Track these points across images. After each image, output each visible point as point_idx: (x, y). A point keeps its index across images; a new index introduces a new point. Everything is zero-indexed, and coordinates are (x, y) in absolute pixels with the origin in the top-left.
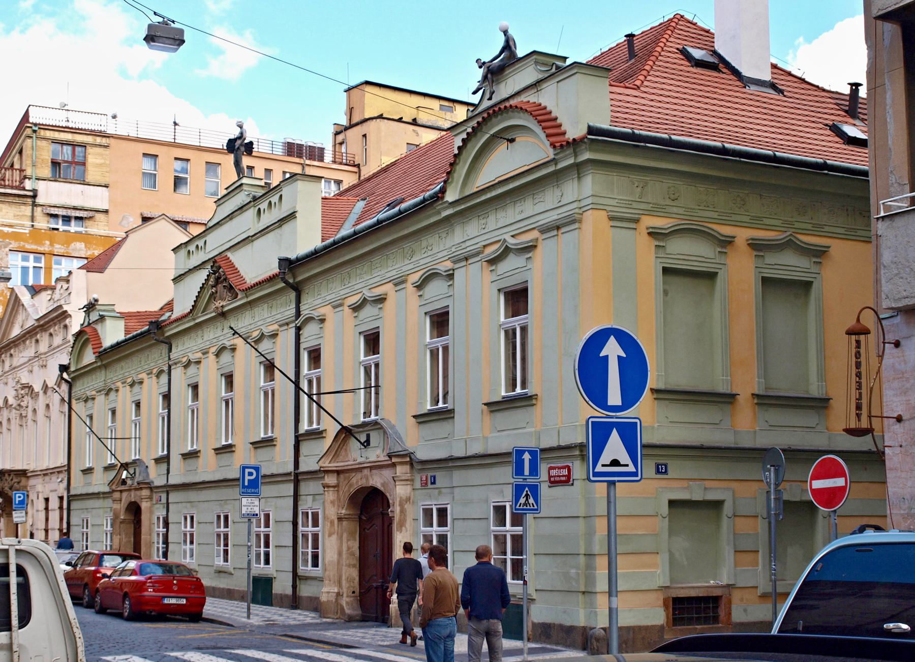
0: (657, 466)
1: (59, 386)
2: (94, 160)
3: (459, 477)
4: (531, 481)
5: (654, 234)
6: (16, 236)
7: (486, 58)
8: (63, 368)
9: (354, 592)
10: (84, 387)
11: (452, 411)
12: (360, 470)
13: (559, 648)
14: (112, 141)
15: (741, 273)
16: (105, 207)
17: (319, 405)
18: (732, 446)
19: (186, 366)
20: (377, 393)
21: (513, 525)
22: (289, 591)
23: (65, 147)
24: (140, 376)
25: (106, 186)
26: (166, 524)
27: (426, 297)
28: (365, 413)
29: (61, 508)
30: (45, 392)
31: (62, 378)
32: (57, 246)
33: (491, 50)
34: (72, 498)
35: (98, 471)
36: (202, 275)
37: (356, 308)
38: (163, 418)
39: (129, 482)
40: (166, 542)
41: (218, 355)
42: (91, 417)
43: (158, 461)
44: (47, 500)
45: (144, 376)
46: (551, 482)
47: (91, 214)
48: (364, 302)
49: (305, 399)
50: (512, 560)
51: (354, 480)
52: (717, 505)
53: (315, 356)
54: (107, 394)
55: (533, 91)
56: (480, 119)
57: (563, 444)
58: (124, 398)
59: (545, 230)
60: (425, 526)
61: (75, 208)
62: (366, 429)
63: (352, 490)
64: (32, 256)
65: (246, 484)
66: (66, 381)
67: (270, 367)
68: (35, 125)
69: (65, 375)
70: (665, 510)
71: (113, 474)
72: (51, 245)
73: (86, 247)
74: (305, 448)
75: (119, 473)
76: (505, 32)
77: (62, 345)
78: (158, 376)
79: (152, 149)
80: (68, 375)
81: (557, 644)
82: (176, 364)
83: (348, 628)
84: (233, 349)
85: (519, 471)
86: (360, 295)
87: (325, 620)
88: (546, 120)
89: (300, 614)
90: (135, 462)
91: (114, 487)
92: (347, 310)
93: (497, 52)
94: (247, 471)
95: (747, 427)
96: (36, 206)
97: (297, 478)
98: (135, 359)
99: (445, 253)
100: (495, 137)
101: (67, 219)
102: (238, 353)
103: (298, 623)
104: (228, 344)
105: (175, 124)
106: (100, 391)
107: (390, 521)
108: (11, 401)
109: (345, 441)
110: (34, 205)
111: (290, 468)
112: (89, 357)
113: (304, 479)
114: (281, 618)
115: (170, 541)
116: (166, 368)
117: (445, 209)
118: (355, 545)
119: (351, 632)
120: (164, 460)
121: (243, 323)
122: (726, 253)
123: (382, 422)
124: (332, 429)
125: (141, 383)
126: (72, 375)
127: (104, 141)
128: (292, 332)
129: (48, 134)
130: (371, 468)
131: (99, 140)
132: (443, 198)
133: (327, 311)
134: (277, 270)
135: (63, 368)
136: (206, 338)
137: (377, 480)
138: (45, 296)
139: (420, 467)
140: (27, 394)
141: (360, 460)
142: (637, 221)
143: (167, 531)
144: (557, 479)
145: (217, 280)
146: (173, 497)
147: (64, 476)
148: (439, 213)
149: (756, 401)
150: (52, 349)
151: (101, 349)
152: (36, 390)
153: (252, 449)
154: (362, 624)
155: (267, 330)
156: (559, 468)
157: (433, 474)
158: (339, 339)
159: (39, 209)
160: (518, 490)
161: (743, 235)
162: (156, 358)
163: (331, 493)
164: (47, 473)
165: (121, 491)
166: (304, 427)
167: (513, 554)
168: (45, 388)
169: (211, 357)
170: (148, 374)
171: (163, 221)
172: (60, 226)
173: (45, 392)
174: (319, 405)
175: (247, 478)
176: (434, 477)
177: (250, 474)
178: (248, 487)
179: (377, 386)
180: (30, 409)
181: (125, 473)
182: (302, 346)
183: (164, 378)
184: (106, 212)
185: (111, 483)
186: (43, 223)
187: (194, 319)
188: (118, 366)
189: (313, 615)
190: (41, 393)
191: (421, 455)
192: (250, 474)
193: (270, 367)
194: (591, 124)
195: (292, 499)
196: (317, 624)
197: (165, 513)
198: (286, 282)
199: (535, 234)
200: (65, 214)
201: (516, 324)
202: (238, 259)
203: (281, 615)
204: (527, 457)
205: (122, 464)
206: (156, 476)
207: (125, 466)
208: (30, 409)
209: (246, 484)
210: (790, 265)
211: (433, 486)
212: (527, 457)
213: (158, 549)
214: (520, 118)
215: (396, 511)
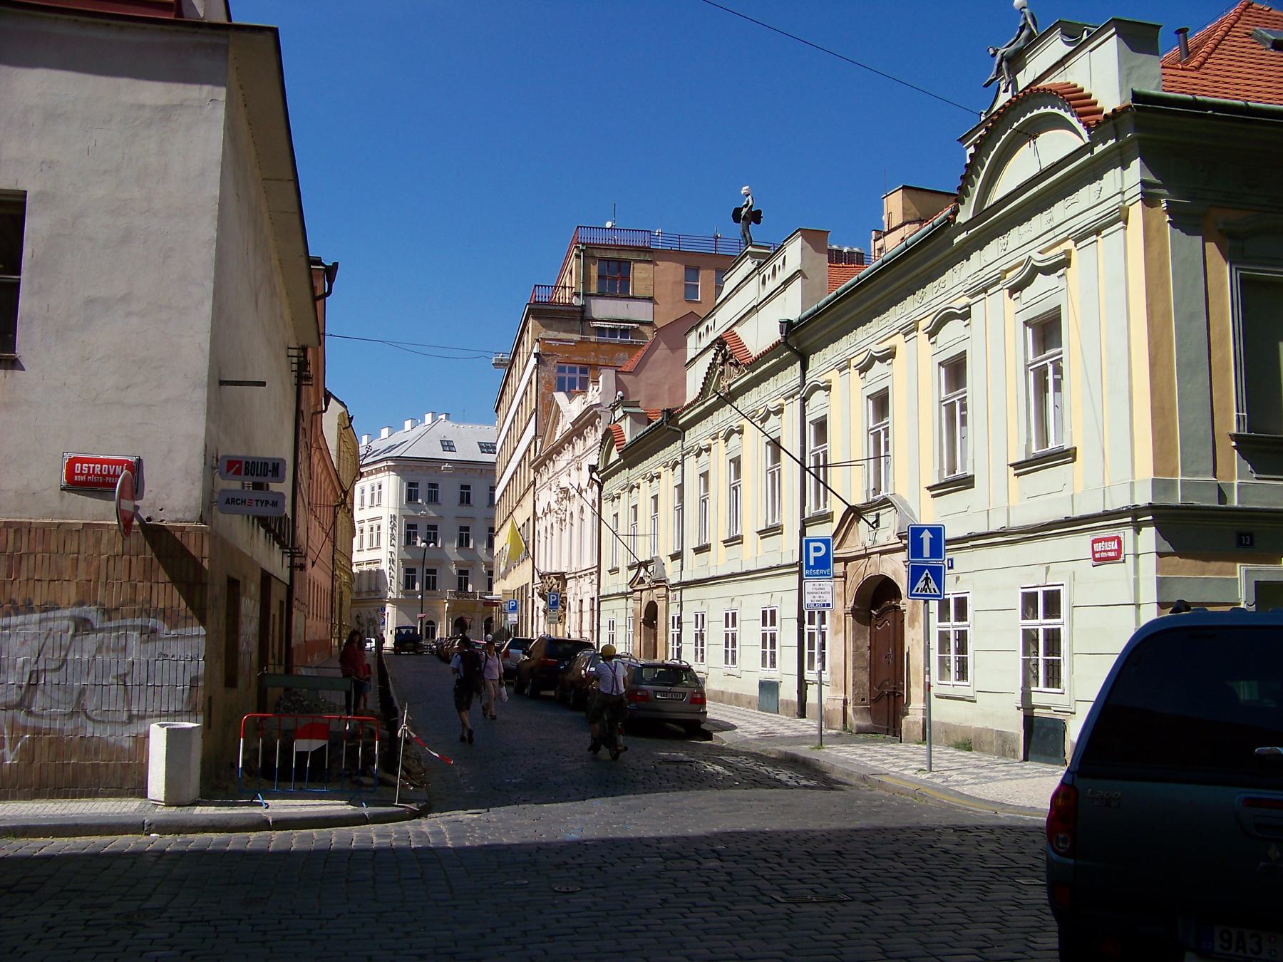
4: (933, 562)
8: (593, 468)
12: (867, 556)
17: (825, 485)
19: (698, 455)
20: (886, 463)
27: (939, 343)
29: (592, 610)
35: (623, 569)
36: (710, 355)
37: (864, 368)
39: (647, 580)
45: (640, 481)
46: (1095, 560)
48: (769, 413)
49: (811, 480)
53: (821, 426)
54: (631, 491)
57: (1109, 508)
58: (643, 496)
59: (1080, 237)
65: (812, 563)
67: (776, 445)
72: (596, 356)
84: (741, 432)
85: (916, 550)
88: (1077, 100)
90: (651, 561)
92: (854, 372)
94: (812, 545)
104: (735, 425)
108: (554, 506)
112: (615, 456)
116: (679, 459)
120: (677, 556)
121: (747, 402)
123: (892, 499)
124: (838, 510)
125: (659, 477)
128: (797, 403)
130: (882, 553)
133: (834, 376)
135: (593, 468)
144: (1104, 555)
145: (724, 356)
146: (688, 593)
150: (587, 451)
151: (393, 590)
155: (772, 405)
156: (1107, 540)
158: (845, 405)
164: (578, 576)
165: (641, 591)
166: (810, 510)
167: (1046, 654)
174: (825, 485)
175: (812, 554)
177: (817, 549)
178: (814, 567)
181: (643, 570)
182: (808, 419)
192: (817, 549)
193: (776, 445)
194: (1136, 89)
199: (1069, 244)
201: (1047, 361)
202: (742, 331)
204: (926, 536)
206: (672, 573)
207: (644, 564)
208: (568, 513)
209: (812, 563)
212: (926, 536)
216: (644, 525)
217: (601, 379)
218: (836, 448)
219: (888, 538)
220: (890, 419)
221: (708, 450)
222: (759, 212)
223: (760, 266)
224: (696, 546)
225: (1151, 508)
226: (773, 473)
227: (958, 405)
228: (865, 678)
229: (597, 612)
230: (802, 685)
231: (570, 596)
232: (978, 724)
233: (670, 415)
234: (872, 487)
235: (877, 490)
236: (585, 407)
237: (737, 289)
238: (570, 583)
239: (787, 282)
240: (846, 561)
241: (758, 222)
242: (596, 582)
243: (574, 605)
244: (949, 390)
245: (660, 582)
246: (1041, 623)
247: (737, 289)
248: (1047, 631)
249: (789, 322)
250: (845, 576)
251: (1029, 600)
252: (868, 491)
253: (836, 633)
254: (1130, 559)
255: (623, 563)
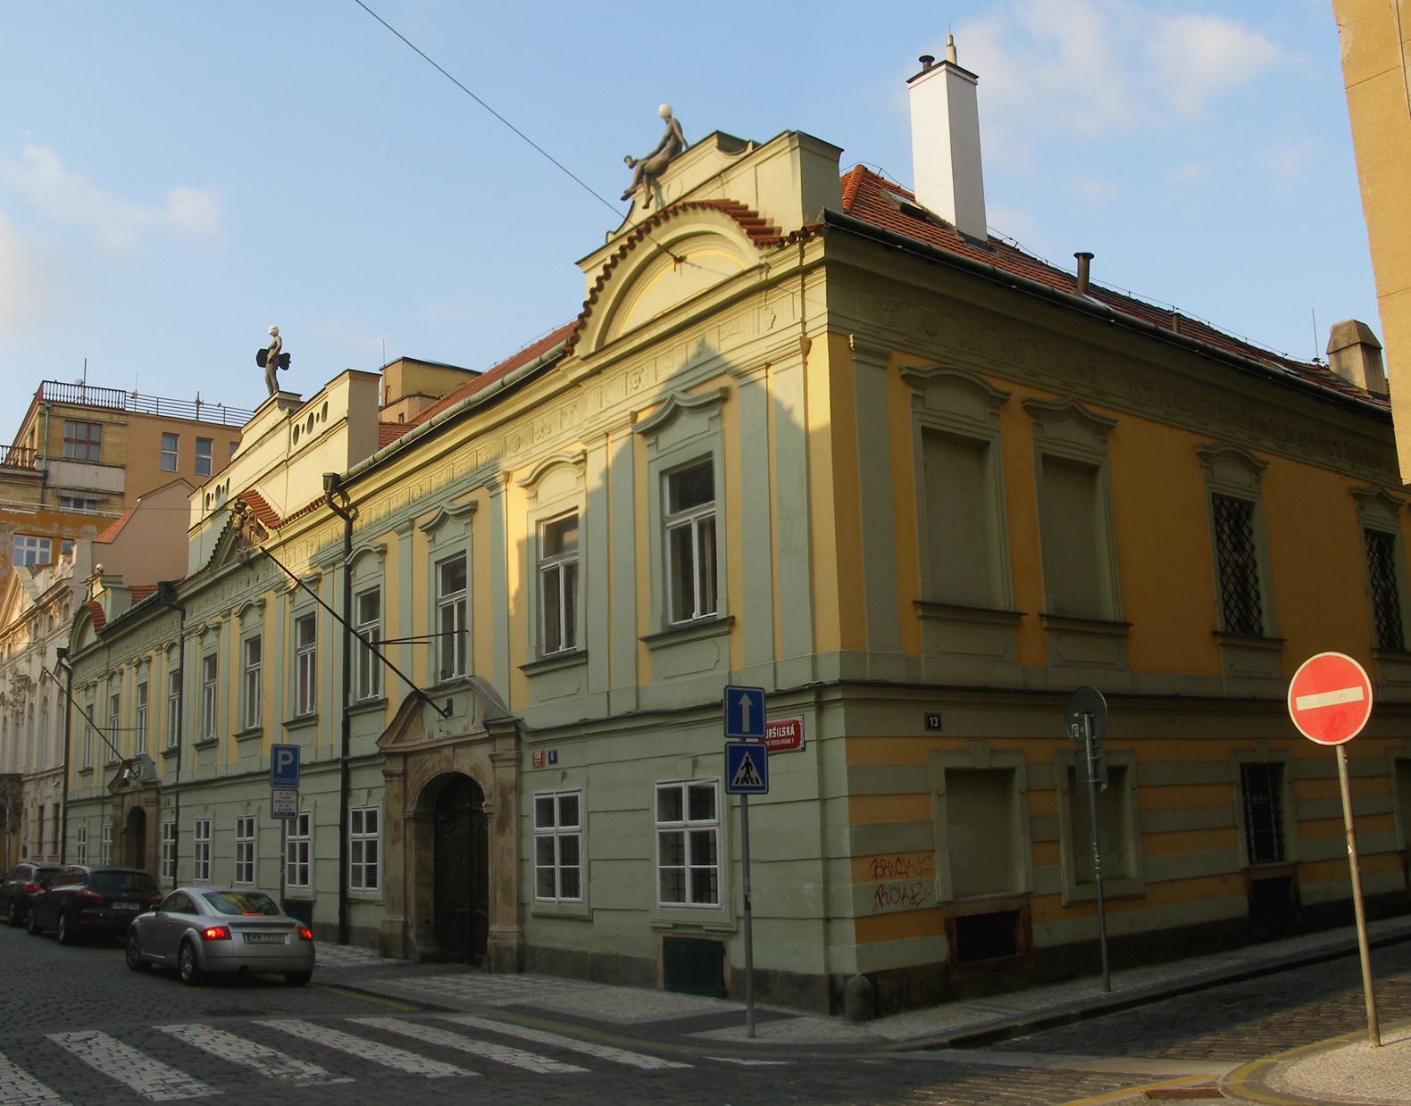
0: (928, 717)
1: (58, 676)
2: (110, 439)
3: (596, 750)
5: (910, 378)
6: (23, 518)
7: (640, 154)
8: (62, 653)
9: (427, 921)
10: (87, 672)
11: (585, 654)
13: (786, 1010)
14: (131, 420)
15: (1016, 444)
16: (121, 489)
18: (1021, 688)
19: (203, 635)
21: (563, 823)
22: (335, 920)
23: (80, 426)
24: (148, 654)
25: (122, 467)
26: (175, 834)
28: (443, 672)
30: (43, 683)
31: (62, 665)
32: (66, 529)
33: (647, 143)
34: (69, 805)
37: (431, 529)
38: (174, 703)
39: (133, 783)
40: (175, 855)
41: (242, 615)
42: (90, 707)
43: (167, 755)
44: (42, 808)
45: (152, 653)
47: (105, 497)
48: (444, 518)
50: (693, 871)
51: (429, 765)
52: (1003, 777)
53: (372, 602)
54: (110, 679)
55: (715, 186)
56: (625, 242)
58: (127, 686)
60: (539, 825)
61: (88, 491)
62: (448, 692)
63: (427, 779)
64: (38, 541)
65: (280, 771)
66: (65, 667)
68: (49, 401)
69: (64, 661)
70: (939, 782)
71: (113, 774)
72: (60, 528)
73: (98, 530)
74: (358, 725)
75: (121, 773)
76: (668, 117)
77: (63, 627)
78: (169, 651)
79: (174, 429)
80: (68, 660)
81: (783, 1003)
82: (190, 633)
83: (426, 974)
84: (262, 605)
85: (734, 726)
86: (439, 509)
87: (387, 960)
89: (351, 952)
90: (138, 759)
91: (115, 790)
92: (419, 535)
93: (655, 147)
94: (281, 753)
95: (1035, 659)
96: (47, 488)
97: (346, 766)
98: (142, 634)
99: (572, 433)
100: (664, 249)
101: (79, 503)
102: (269, 609)
103: (351, 965)
104: (254, 600)
105: (198, 403)
106: (102, 677)
107: (484, 818)
109: (420, 706)
110: (45, 487)
111: (338, 753)
112: (91, 637)
113: (357, 768)
114: (326, 957)
115: (179, 854)
116: (177, 641)
117: (579, 366)
118: (429, 855)
119: (436, 981)
120: (173, 753)
122: (998, 415)
126: (72, 661)
127: (122, 419)
129: (62, 411)
130: (454, 746)
131: (116, 418)
132: (572, 352)
134: (323, 493)
135: (62, 653)
136: (226, 598)
137: (464, 763)
138: (45, 573)
139: (531, 740)
140: (24, 688)
141: (437, 735)
142: (886, 357)
143: (177, 842)
144: (777, 742)
146: (185, 799)
147: (61, 779)
148: (564, 376)
149: (1045, 624)
152: (33, 682)
153: (285, 732)
154: (441, 967)
157: (554, 748)
159: (50, 491)
160: (734, 756)
161: (1018, 393)
162: (167, 628)
163: (395, 783)
164: (40, 777)
166: (356, 696)
168: (43, 679)
169: (235, 620)
170: (157, 650)
171: (182, 486)
172: (71, 509)
173: (43, 683)
175: (281, 763)
176: (555, 753)
177: (285, 758)
178: (281, 776)
179: (462, 631)
180: (27, 705)
182: (354, 591)
183: (176, 653)
184: (122, 495)
185: (111, 786)
186: (52, 504)
187: (213, 575)
188: (122, 645)
189: (369, 952)
190: (39, 684)
191: (533, 722)
192: (285, 758)
195: (339, 796)
196: (377, 967)
197: (174, 820)
198: (333, 506)
200: (77, 496)
203: (326, 953)
204: (746, 702)
205: (124, 761)
206: (164, 773)
207: (128, 764)
208: (27, 705)
209: (280, 771)
210: (1073, 440)
211: (552, 766)
212: (746, 702)
213: (165, 863)
214: (698, 222)
215: (490, 804)
216: (128, 716)
217: (75, 549)
218: (391, 622)
219: (466, 729)
220: (467, 593)
221: (218, 628)
222: (287, 356)
223: (291, 413)
224: (198, 741)
225: (842, 684)
226: (210, 691)
227: (309, 656)
228: (429, 895)
229: (61, 820)
230: (346, 903)
231: (27, 804)
232: (597, 949)
233: (169, 589)
234: (440, 670)
235: (446, 672)
236: (53, 582)
237: (260, 441)
238: (29, 788)
239: (327, 432)
240: (406, 755)
241: (285, 367)
242: (62, 785)
243: (32, 813)
244: (303, 642)
245: (152, 786)
246: (687, 825)
247: (260, 441)
248: (563, 839)
249: (336, 477)
250: (405, 773)
251: (670, 801)
252: (436, 674)
253: (394, 842)
254: (812, 748)
255: (97, 763)
